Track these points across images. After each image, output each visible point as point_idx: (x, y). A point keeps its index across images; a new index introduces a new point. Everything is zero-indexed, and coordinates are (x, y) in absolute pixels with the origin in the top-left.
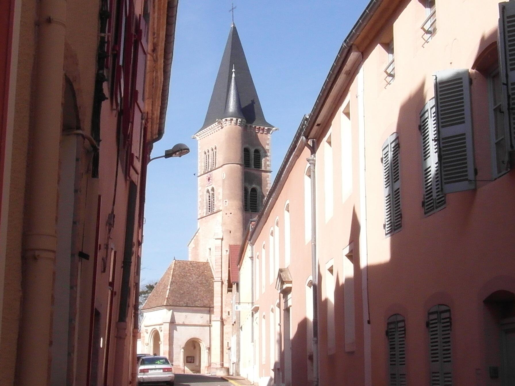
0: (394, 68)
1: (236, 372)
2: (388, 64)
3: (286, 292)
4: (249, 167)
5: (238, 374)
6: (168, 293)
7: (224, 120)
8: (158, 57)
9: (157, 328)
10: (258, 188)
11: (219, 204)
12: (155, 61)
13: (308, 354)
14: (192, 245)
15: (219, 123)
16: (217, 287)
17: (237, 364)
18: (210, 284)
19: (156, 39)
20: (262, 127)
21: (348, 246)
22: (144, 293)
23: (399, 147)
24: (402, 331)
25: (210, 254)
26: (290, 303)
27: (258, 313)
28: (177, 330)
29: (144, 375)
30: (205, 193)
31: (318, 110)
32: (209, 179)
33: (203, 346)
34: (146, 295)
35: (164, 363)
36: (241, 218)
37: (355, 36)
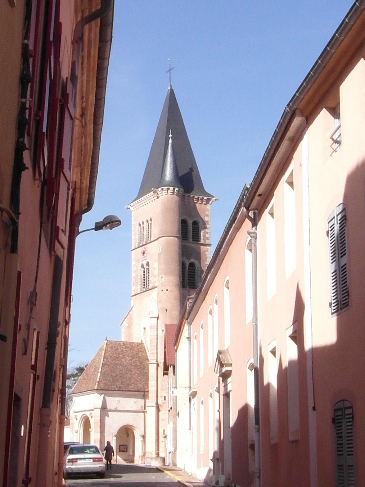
0: (340, 135)
1: (173, 462)
2: (334, 130)
3: (225, 376)
4: (186, 240)
5: (175, 465)
6: (99, 376)
7: (160, 189)
8: (88, 121)
9: (88, 414)
10: (196, 262)
11: (154, 280)
12: (84, 126)
13: (249, 443)
14: (125, 324)
15: (155, 192)
16: (152, 370)
17: (174, 453)
18: (144, 365)
19: (84, 103)
20: (201, 197)
21: (292, 326)
22: (74, 376)
23: (345, 219)
24: (349, 418)
25: (145, 334)
26: (229, 388)
27: (195, 399)
28: (108, 416)
29: (72, 465)
30: (140, 268)
31: (259, 179)
32: (144, 253)
33: (137, 434)
34: (76, 378)
35: (94, 452)
36: (178, 295)
37: (300, 100)
